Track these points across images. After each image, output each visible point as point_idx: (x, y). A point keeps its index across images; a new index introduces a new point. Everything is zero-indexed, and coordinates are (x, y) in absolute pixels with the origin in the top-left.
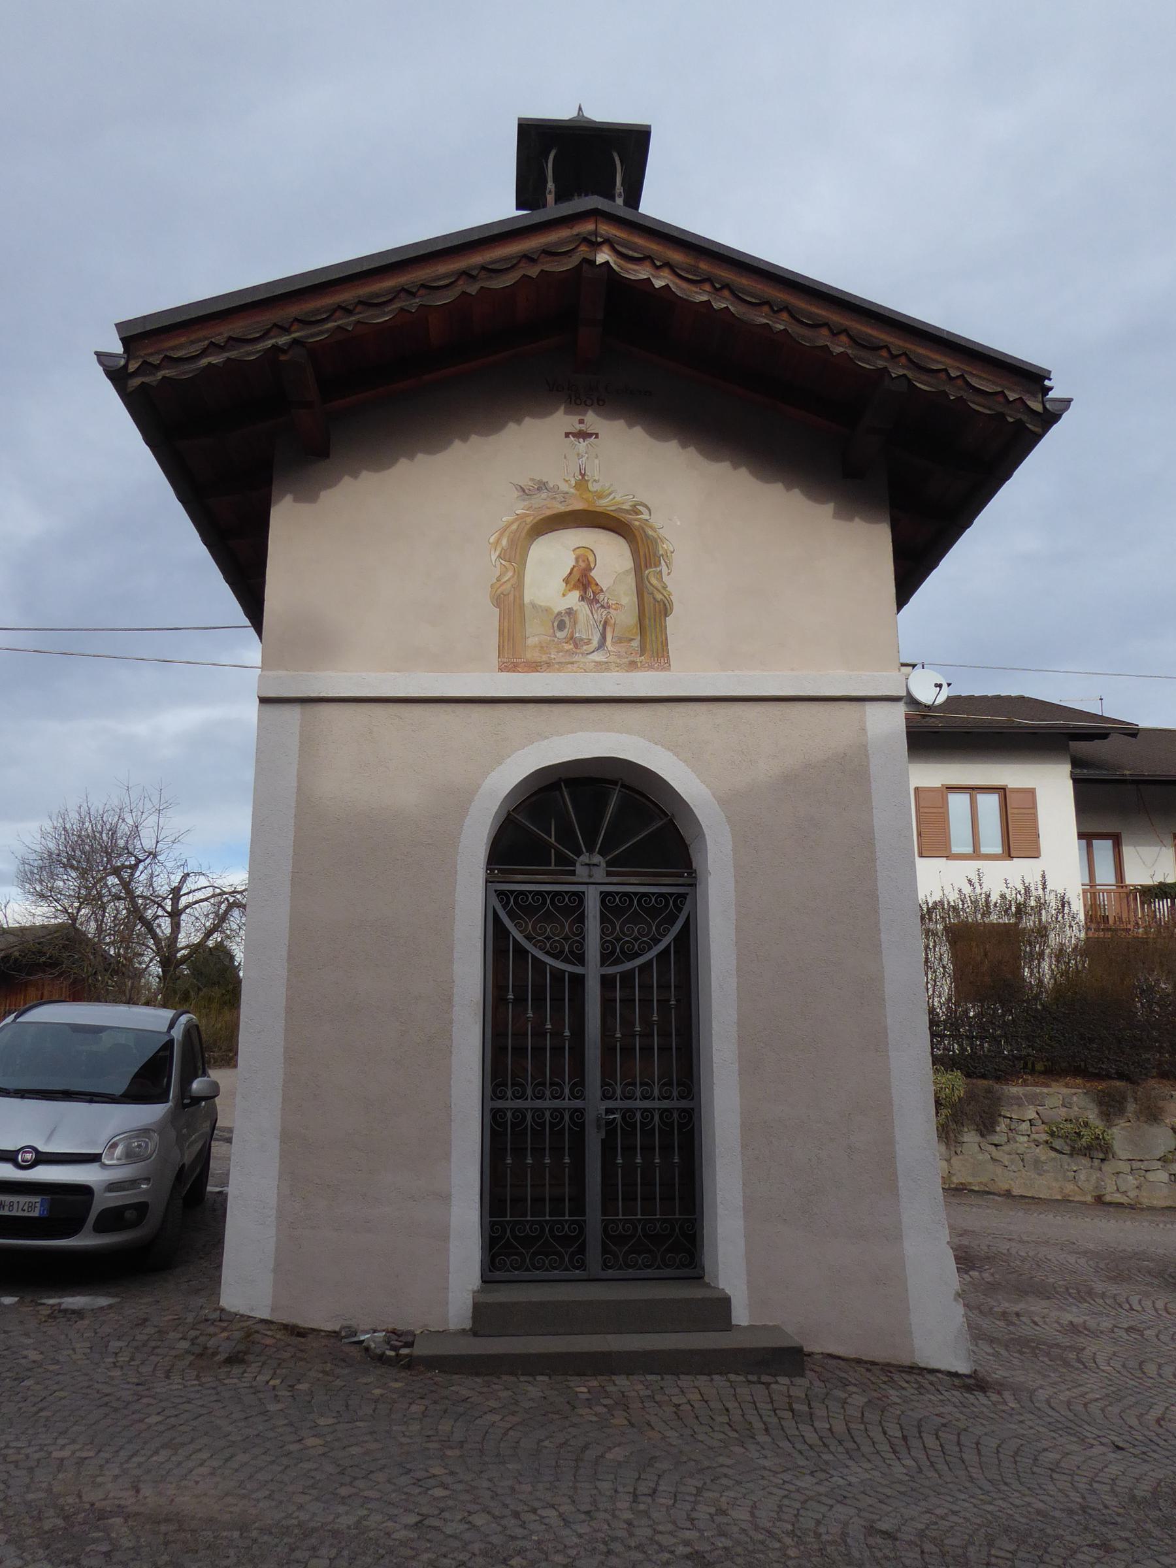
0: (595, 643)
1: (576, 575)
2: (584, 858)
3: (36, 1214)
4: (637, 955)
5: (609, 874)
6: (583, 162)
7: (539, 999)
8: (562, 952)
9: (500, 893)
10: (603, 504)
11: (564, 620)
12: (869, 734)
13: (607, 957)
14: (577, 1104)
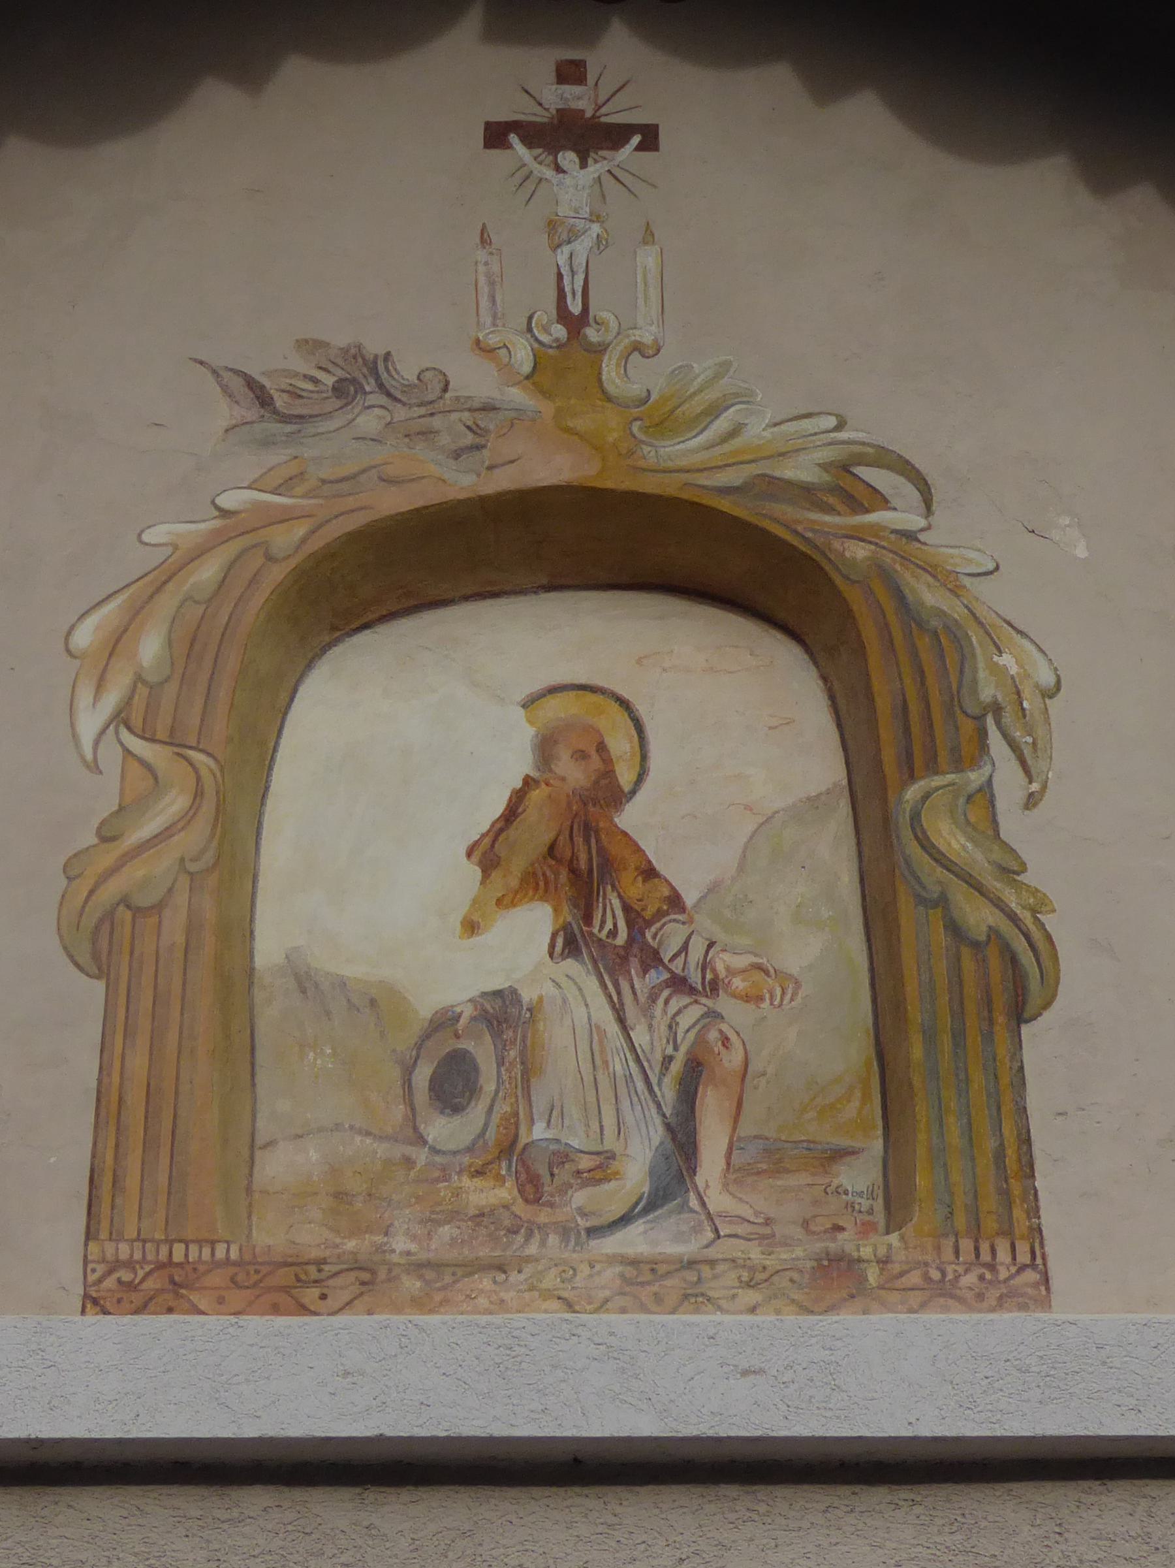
1: (537, 828)
11: (461, 1058)
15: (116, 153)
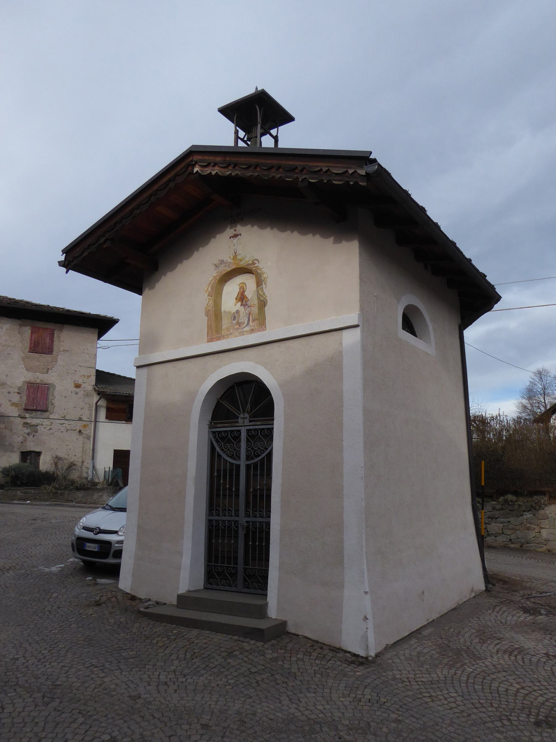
0: (246, 323)
1: (240, 296)
2: (242, 416)
3: (96, 550)
4: (259, 456)
5: (250, 421)
6: (256, 111)
8: (233, 455)
10: (242, 264)
11: (235, 316)
12: (344, 345)
13: (248, 458)
14: (237, 518)
15: (207, 247)
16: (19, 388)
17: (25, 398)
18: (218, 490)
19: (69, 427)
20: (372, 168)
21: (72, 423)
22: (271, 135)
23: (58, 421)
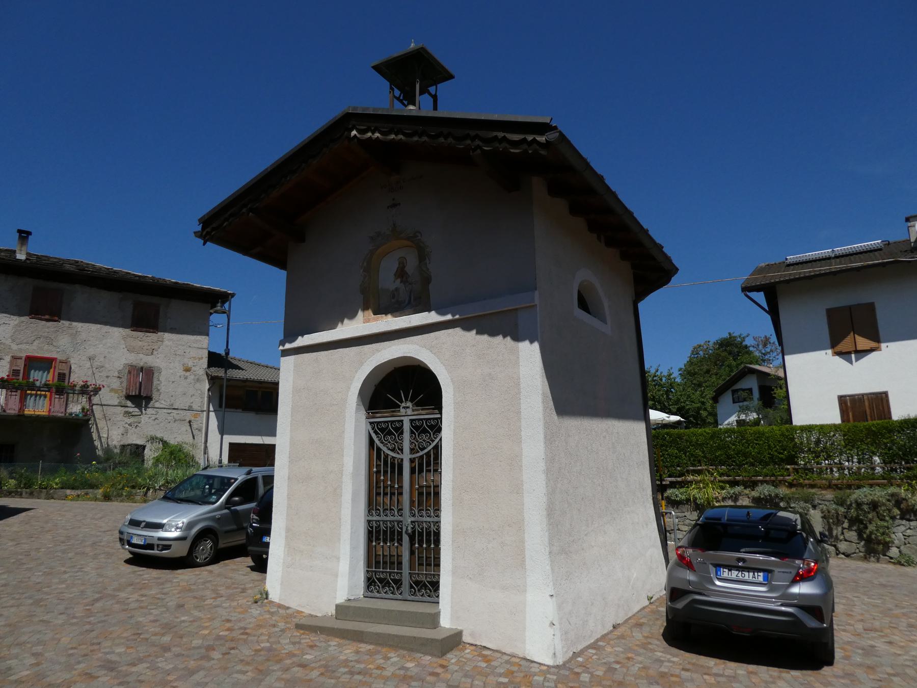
2: (403, 405)
4: (424, 448)
6: (414, 71)
7: (386, 472)
9: (371, 423)
13: (412, 451)
16: (119, 372)
17: (125, 385)
18: (378, 487)
19: (177, 417)
20: (552, 136)
21: (181, 412)
22: (430, 94)
23: (165, 411)
